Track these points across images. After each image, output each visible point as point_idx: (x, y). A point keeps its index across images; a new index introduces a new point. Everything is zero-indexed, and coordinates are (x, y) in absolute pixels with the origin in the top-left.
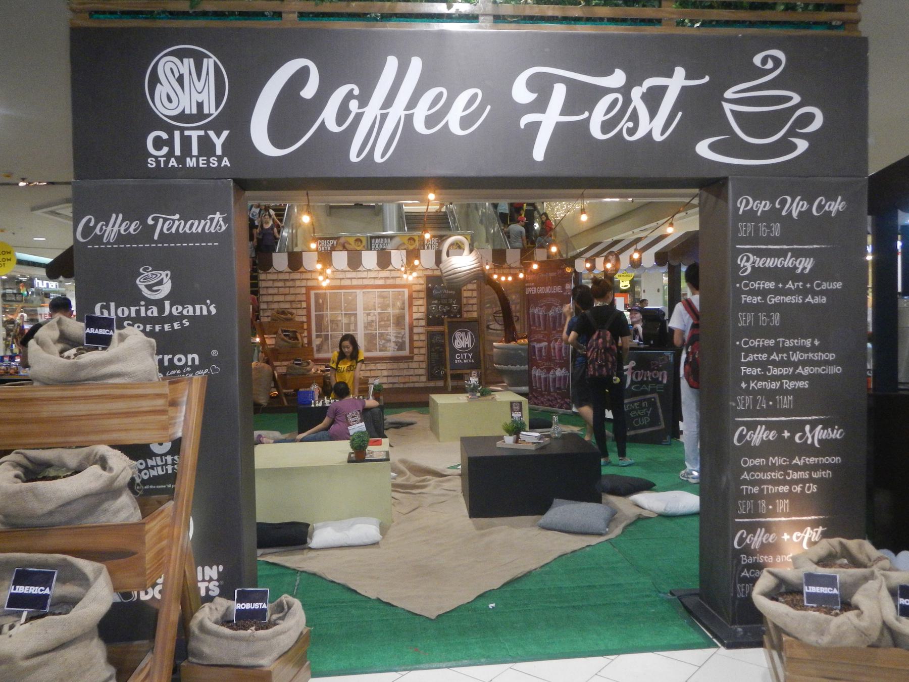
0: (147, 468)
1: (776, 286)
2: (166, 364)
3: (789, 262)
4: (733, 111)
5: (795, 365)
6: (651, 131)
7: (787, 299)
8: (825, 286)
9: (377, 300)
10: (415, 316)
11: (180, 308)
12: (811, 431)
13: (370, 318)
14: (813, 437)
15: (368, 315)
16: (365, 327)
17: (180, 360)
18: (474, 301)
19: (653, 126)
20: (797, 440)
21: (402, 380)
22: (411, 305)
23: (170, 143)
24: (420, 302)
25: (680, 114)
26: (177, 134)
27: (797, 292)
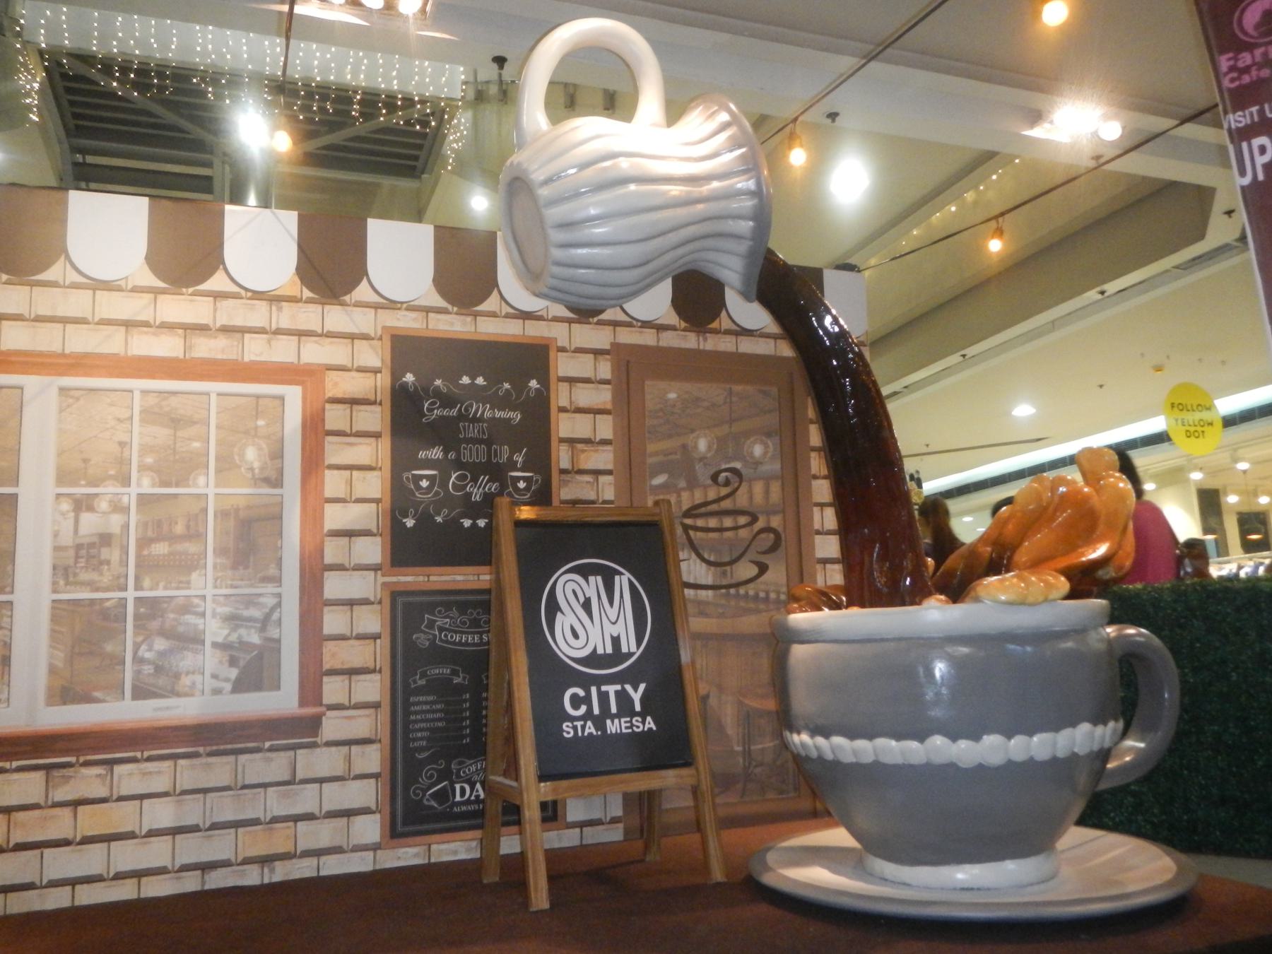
9: (139, 434)
10: (335, 517)
13: (90, 523)
15: (82, 505)
16: (63, 573)
18: (602, 459)
21: (255, 843)
22: (313, 463)
23: (587, 700)
24: (363, 452)
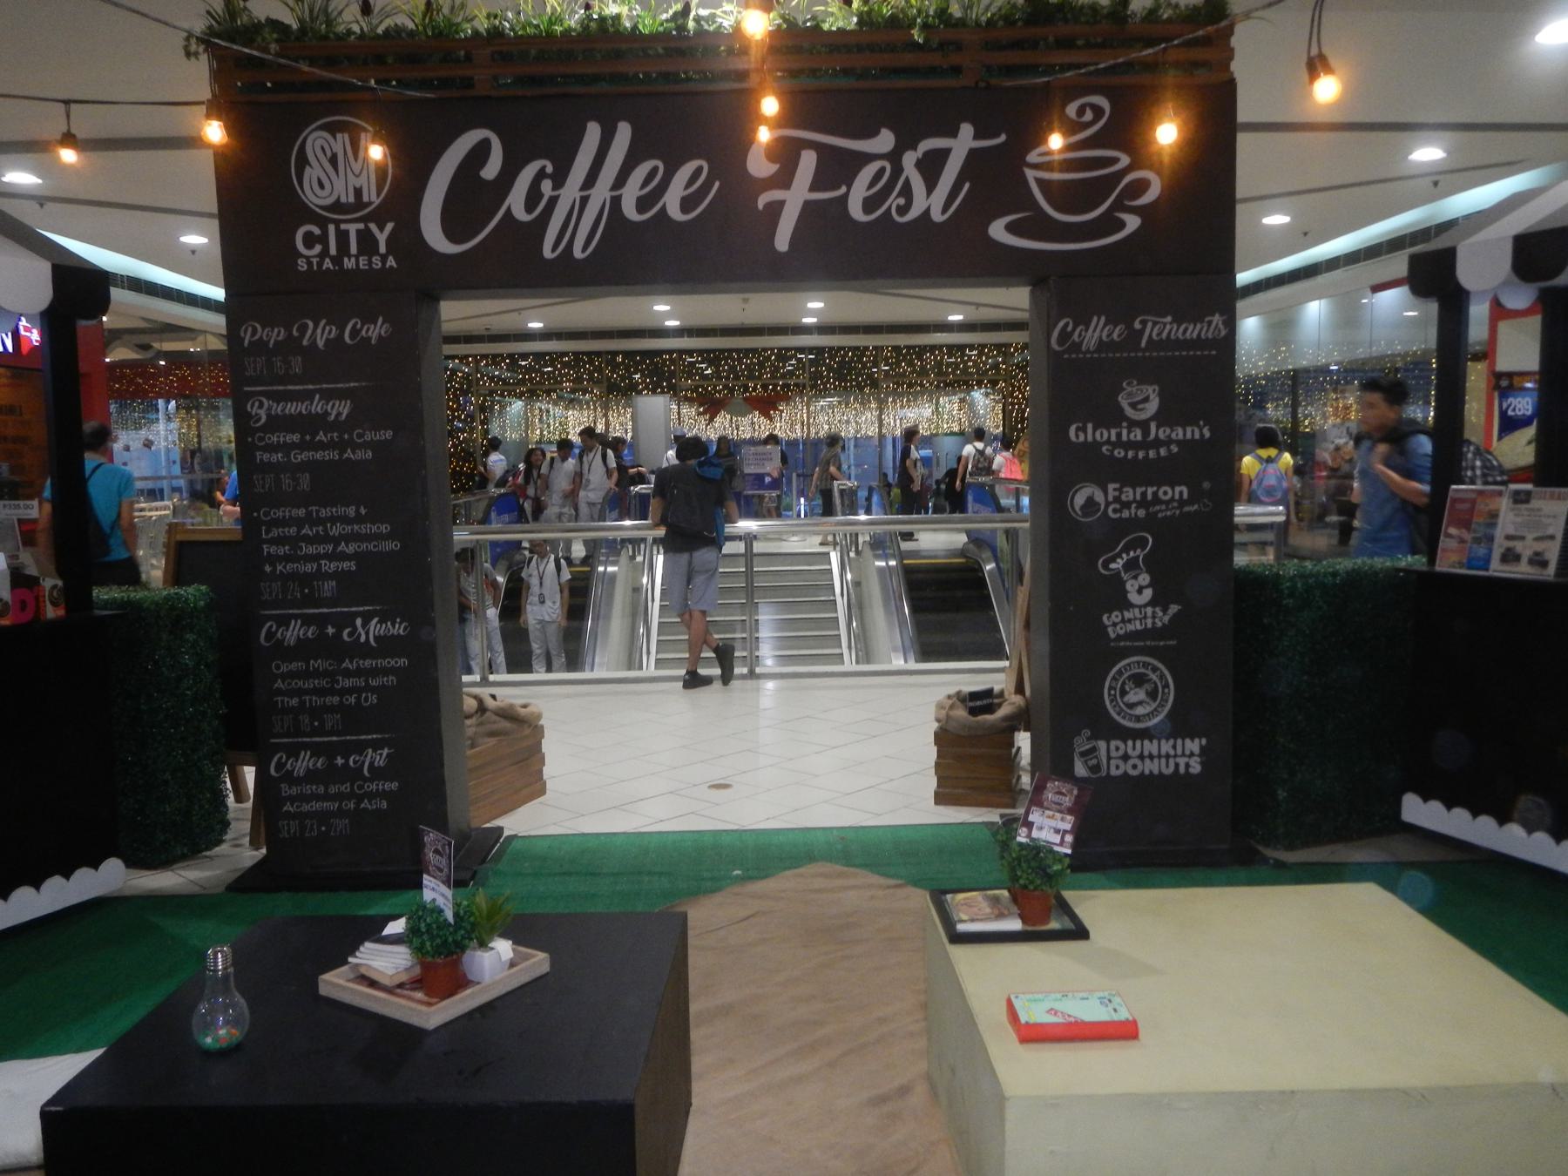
0: (1123, 621)
1: (302, 438)
2: (1149, 497)
3: (317, 406)
4: (1038, 180)
5: (336, 541)
6: (928, 209)
7: (318, 456)
8: (369, 436)
11: (1168, 431)
12: (364, 626)
14: (367, 634)
17: (1165, 493)
19: (931, 203)
20: (345, 637)
23: (324, 240)
25: (967, 185)
26: (331, 228)
27: (331, 445)
